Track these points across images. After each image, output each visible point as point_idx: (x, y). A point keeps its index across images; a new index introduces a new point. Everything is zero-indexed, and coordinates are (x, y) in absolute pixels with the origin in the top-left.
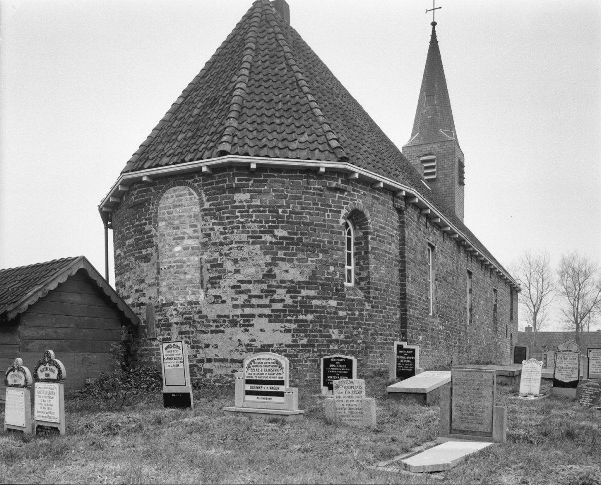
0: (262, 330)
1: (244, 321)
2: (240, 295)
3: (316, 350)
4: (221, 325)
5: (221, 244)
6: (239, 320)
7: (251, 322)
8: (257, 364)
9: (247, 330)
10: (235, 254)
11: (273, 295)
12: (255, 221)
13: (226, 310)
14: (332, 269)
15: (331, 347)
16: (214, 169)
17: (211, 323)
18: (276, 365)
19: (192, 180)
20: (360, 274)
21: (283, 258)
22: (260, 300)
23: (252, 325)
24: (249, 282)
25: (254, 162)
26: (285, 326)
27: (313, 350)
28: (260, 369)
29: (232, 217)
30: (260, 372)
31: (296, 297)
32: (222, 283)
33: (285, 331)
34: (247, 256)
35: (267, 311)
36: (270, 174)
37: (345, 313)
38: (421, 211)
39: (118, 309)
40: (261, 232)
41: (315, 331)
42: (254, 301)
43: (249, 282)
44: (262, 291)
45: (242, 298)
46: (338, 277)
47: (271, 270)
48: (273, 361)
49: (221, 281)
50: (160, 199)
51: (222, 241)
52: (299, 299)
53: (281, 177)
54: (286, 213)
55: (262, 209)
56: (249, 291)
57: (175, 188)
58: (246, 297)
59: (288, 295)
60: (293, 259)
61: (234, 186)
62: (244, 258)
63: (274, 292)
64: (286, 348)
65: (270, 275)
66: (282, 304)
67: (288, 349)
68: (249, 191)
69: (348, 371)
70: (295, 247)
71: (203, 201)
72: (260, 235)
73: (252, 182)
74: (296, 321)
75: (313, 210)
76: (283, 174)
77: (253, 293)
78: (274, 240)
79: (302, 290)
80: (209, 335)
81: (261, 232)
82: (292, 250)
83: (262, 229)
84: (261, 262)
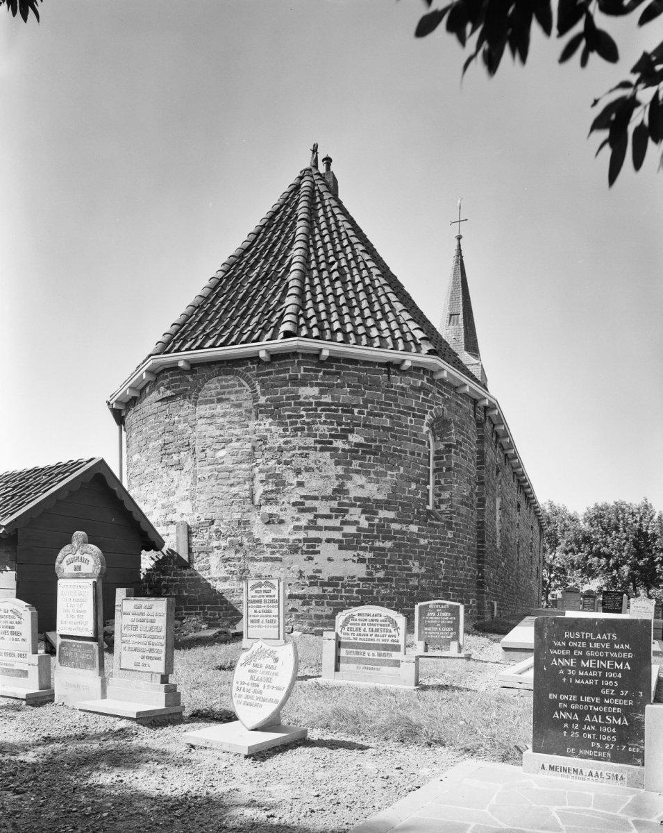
0: (329, 559)
1: (308, 547)
2: (303, 514)
3: (394, 586)
4: (278, 552)
5: (281, 450)
6: (300, 545)
7: (317, 549)
8: (358, 622)
9: (311, 559)
10: (299, 462)
11: (344, 516)
12: (325, 422)
13: (286, 532)
14: (413, 486)
15: (411, 583)
16: (275, 357)
17: (265, 549)
18: (387, 623)
19: (243, 368)
20: (440, 495)
21: (357, 470)
22: (329, 520)
23: (318, 552)
24: (315, 498)
25: (327, 349)
26: (358, 555)
27: (391, 585)
28: (363, 628)
29: (295, 415)
30: (362, 632)
31: (372, 519)
32: (283, 499)
33: (358, 560)
34: (313, 465)
35: (337, 535)
36: (343, 364)
37: (426, 541)
38: (494, 427)
39: (108, 487)
40: (332, 436)
41: (394, 562)
42: (321, 522)
43: (315, 498)
44: (331, 510)
45: (305, 519)
46: (419, 496)
47: (342, 485)
48: (383, 618)
49: (278, 496)
50: (200, 390)
51: (282, 445)
52: (376, 521)
53: (355, 369)
54: (363, 414)
55: (333, 407)
56: (315, 509)
57: (220, 378)
58: (310, 516)
59: (363, 516)
60: (370, 471)
61: (299, 377)
62: (310, 468)
63: (347, 511)
64: (359, 582)
65: (340, 490)
66: (355, 527)
67: (361, 583)
68: (317, 385)
69: (624, 672)
70: (372, 457)
71: (257, 395)
72: (331, 439)
73: (321, 374)
74: (372, 549)
75: (395, 412)
76: (359, 366)
77: (320, 512)
78: (347, 447)
79: (380, 511)
80: (262, 564)
81: (332, 436)
82: (369, 460)
83: (333, 432)
84: (330, 474)
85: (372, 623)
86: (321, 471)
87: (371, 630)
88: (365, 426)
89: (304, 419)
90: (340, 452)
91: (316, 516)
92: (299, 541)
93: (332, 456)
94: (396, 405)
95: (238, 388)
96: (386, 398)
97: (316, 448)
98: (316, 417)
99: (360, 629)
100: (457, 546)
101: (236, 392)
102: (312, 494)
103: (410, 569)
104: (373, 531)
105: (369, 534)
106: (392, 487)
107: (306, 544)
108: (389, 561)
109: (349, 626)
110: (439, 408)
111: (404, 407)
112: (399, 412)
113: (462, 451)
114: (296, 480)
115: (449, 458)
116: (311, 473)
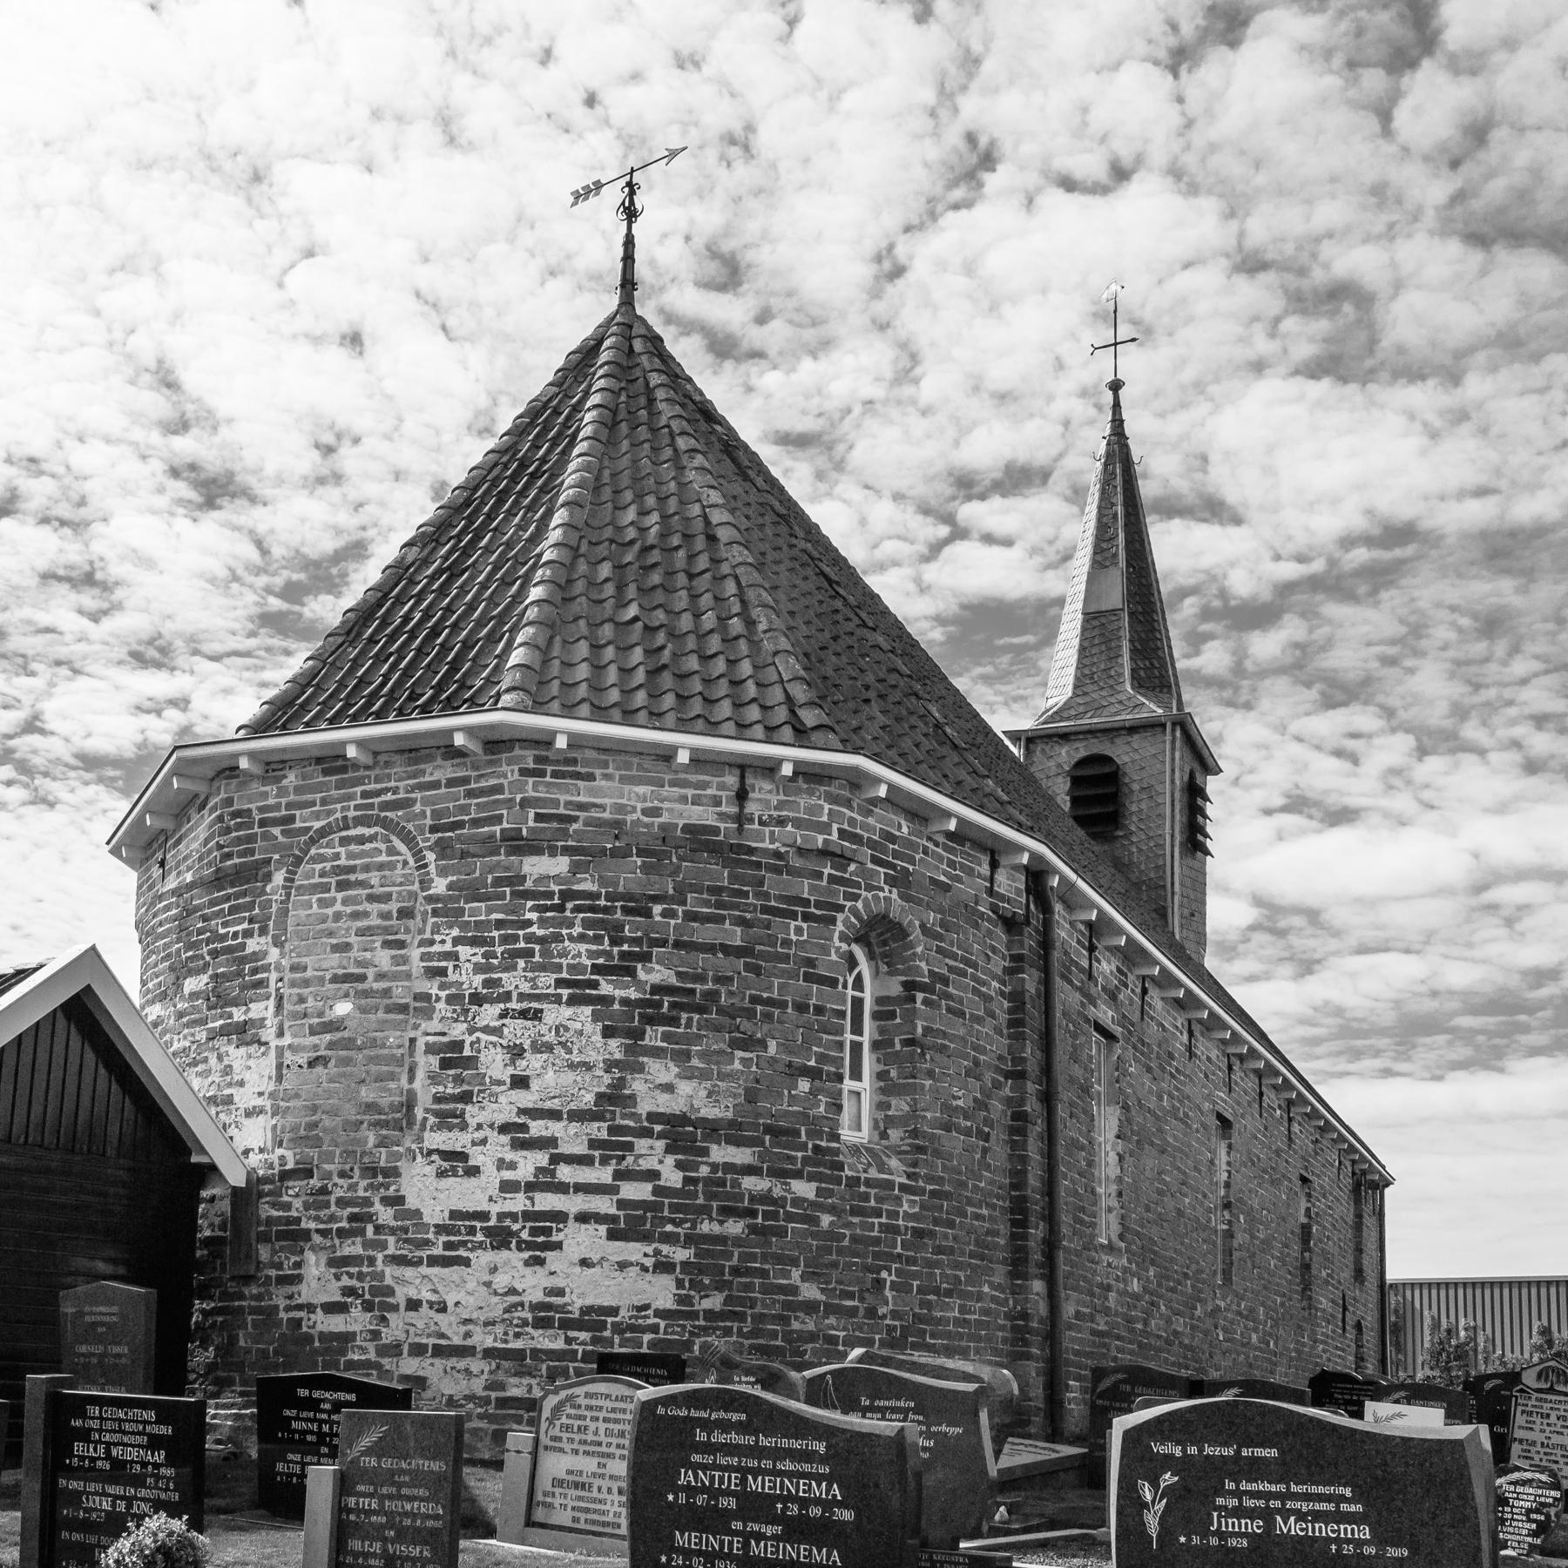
0: (585, 1263)
1: (534, 1232)
2: (524, 1153)
8: (583, 1412)
9: (540, 1262)
11: (623, 1158)
12: (582, 938)
23: (558, 1246)
24: (554, 1115)
26: (657, 1252)
28: (592, 1426)
29: (512, 922)
30: (590, 1437)
32: (473, 1114)
35: (604, 1205)
40: (597, 969)
42: (565, 1173)
44: (593, 1144)
45: (528, 1164)
47: (620, 1083)
49: (469, 1108)
50: (298, 861)
52: (704, 1171)
56: (551, 1142)
59: (670, 1160)
61: (524, 832)
64: (657, 1320)
65: (614, 1098)
66: (649, 1187)
67: (662, 1324)
68: (567, 851)
70: (696, 1017)
71: (428, 873)
74: (690, 1240)
75: (755, 910)
77: (565, 1149)
78: (633, 994)
79: (714, 1148)
83: (601, 961)
84: (592, 1056)
85: (612, 1415)
86: (570, 1052)
87: (608, 1433)
88: (678, 945)
89: (534, 929)
90: (616, 1006)
91: (556, 1159)
92: (513, 1216)
93: (596, 1017)
94: (757, 895)
95: (383, 858)
96: (734, 878)
97: (560, 996)
98: (560, 925)
99: (586, 1428)
100: (932, 1234)
101: (381, 867)
102: (548, 1105)
103: (794, 1290)
104: (695, 1195)
105: (683, 1203)
106: (747, 1090)
107: (528, 1225)
108: (736, 1271)
109: (564, 1420)
110: (876, 898)
111: (780, 898)
112: (766, 910)
113: (949, 996)
114: (511, 1071)
115: (911, 1016)
116: (545, 1056)
